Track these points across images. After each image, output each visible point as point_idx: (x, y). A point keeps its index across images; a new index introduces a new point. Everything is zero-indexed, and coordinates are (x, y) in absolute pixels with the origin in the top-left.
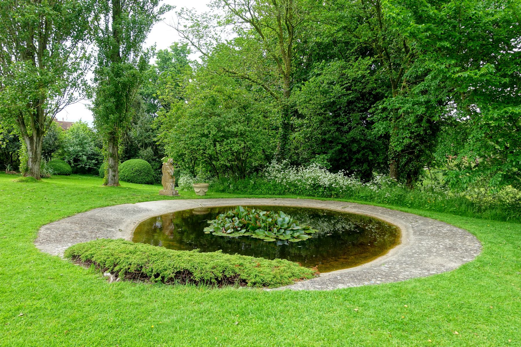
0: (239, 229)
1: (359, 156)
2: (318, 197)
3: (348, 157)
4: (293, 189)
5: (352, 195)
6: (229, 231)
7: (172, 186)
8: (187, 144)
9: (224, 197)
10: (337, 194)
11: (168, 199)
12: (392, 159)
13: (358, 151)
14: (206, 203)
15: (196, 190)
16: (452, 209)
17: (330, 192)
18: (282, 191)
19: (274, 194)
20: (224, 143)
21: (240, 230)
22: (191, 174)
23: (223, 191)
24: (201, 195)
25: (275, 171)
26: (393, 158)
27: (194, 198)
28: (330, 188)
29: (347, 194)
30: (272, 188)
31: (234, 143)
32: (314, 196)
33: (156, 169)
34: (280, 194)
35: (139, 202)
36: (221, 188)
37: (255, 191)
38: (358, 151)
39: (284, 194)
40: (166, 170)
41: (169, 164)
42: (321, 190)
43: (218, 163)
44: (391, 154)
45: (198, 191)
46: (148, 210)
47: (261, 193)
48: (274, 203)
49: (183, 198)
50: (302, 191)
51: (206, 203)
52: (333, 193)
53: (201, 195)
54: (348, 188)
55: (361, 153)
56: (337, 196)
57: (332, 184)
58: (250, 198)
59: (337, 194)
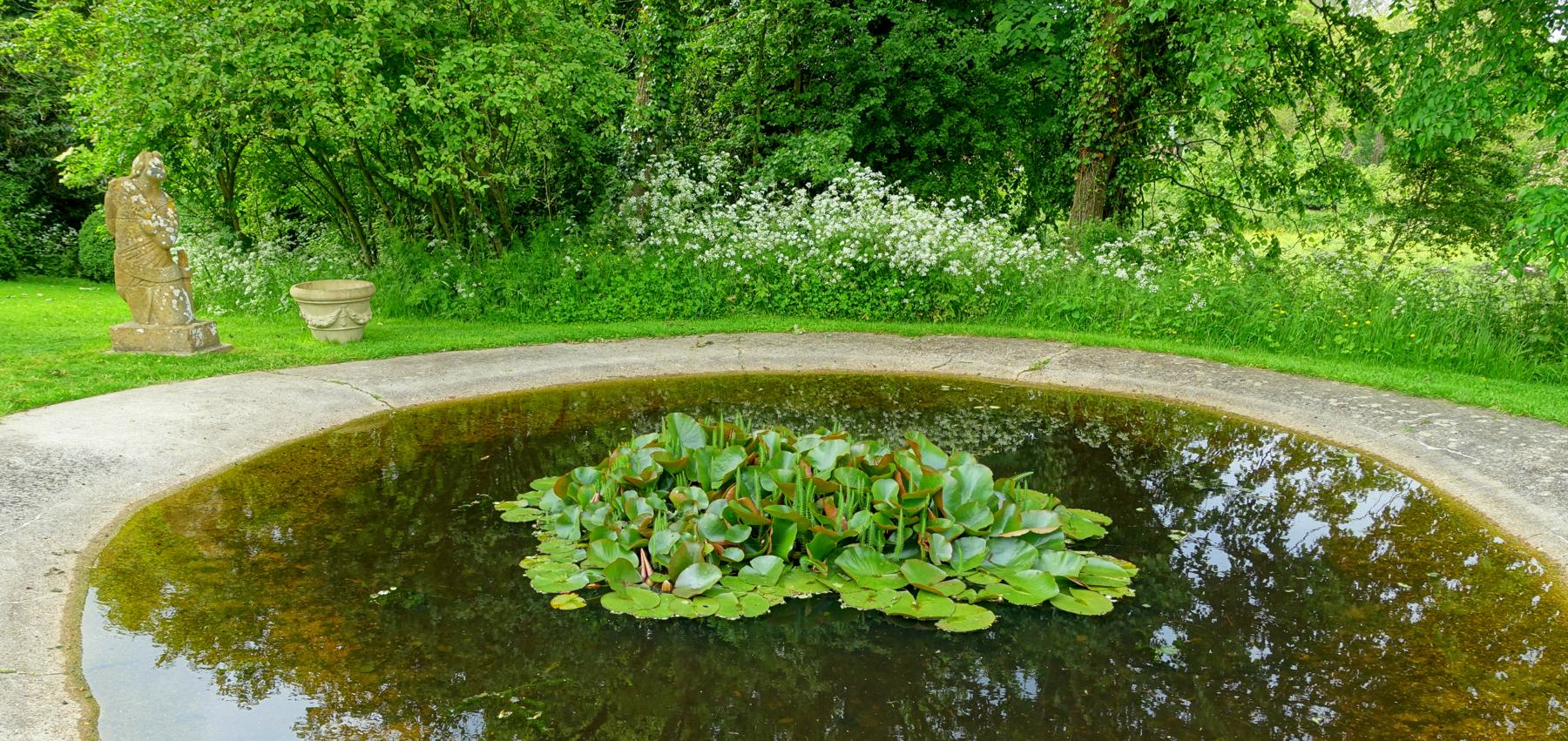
0: (736, 555)
1: (936, 138)
2: (874, 318)
3: (896, 144)
4: (772, 293)
5: (1017, 308)
6: (692, 579)
7: (182, 305)
8: (231, 68)
9: (460, 341)
10: (956, 306)
11: (180, 376)
12: (1092, 149)
13: (934, 120)
14: (399, 387)
15: (313, 317)
16: (1438, 350)
17: (930, 298)
18: (717, 300)
19: (677, 313)
20: (444, 69)
21: (746, 561)
22: (225, 232)
23: (427, 309)
24: (343, 338)
25: (671, 206)
26: (1097, 142)
27: (318, 361)
28: (934, 281)
29: (1004, 303)
30: (668, 286)
31: (492, 68)
32: (856, 316)
33: (15, 210)
34: (706, 314)
35: (21, 406)
36: (416, 295)
37: (585, 307)
38: (934, 120)
39: (723, 311)
40: (131, 217)
41: (144, 183)
42: (892, 288)
43: (421, 176)
44: (1086, 127)
45: (326, 318)
46: (100, 463)
47: (617, 315)
48: (717, 360)
49: (256, 365)
50: (801, 298)
51: (399, 387)
52: (944, 299)
53: (343, 338)
54: (1011, 276)
55: (946, 123)
56: (959, 312)
57: (945, 263)
58: (584, 340)
59: (956, 306)
